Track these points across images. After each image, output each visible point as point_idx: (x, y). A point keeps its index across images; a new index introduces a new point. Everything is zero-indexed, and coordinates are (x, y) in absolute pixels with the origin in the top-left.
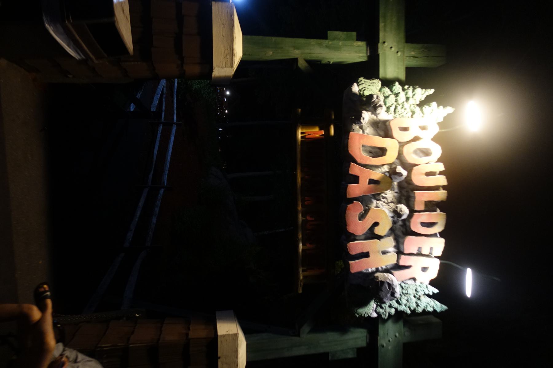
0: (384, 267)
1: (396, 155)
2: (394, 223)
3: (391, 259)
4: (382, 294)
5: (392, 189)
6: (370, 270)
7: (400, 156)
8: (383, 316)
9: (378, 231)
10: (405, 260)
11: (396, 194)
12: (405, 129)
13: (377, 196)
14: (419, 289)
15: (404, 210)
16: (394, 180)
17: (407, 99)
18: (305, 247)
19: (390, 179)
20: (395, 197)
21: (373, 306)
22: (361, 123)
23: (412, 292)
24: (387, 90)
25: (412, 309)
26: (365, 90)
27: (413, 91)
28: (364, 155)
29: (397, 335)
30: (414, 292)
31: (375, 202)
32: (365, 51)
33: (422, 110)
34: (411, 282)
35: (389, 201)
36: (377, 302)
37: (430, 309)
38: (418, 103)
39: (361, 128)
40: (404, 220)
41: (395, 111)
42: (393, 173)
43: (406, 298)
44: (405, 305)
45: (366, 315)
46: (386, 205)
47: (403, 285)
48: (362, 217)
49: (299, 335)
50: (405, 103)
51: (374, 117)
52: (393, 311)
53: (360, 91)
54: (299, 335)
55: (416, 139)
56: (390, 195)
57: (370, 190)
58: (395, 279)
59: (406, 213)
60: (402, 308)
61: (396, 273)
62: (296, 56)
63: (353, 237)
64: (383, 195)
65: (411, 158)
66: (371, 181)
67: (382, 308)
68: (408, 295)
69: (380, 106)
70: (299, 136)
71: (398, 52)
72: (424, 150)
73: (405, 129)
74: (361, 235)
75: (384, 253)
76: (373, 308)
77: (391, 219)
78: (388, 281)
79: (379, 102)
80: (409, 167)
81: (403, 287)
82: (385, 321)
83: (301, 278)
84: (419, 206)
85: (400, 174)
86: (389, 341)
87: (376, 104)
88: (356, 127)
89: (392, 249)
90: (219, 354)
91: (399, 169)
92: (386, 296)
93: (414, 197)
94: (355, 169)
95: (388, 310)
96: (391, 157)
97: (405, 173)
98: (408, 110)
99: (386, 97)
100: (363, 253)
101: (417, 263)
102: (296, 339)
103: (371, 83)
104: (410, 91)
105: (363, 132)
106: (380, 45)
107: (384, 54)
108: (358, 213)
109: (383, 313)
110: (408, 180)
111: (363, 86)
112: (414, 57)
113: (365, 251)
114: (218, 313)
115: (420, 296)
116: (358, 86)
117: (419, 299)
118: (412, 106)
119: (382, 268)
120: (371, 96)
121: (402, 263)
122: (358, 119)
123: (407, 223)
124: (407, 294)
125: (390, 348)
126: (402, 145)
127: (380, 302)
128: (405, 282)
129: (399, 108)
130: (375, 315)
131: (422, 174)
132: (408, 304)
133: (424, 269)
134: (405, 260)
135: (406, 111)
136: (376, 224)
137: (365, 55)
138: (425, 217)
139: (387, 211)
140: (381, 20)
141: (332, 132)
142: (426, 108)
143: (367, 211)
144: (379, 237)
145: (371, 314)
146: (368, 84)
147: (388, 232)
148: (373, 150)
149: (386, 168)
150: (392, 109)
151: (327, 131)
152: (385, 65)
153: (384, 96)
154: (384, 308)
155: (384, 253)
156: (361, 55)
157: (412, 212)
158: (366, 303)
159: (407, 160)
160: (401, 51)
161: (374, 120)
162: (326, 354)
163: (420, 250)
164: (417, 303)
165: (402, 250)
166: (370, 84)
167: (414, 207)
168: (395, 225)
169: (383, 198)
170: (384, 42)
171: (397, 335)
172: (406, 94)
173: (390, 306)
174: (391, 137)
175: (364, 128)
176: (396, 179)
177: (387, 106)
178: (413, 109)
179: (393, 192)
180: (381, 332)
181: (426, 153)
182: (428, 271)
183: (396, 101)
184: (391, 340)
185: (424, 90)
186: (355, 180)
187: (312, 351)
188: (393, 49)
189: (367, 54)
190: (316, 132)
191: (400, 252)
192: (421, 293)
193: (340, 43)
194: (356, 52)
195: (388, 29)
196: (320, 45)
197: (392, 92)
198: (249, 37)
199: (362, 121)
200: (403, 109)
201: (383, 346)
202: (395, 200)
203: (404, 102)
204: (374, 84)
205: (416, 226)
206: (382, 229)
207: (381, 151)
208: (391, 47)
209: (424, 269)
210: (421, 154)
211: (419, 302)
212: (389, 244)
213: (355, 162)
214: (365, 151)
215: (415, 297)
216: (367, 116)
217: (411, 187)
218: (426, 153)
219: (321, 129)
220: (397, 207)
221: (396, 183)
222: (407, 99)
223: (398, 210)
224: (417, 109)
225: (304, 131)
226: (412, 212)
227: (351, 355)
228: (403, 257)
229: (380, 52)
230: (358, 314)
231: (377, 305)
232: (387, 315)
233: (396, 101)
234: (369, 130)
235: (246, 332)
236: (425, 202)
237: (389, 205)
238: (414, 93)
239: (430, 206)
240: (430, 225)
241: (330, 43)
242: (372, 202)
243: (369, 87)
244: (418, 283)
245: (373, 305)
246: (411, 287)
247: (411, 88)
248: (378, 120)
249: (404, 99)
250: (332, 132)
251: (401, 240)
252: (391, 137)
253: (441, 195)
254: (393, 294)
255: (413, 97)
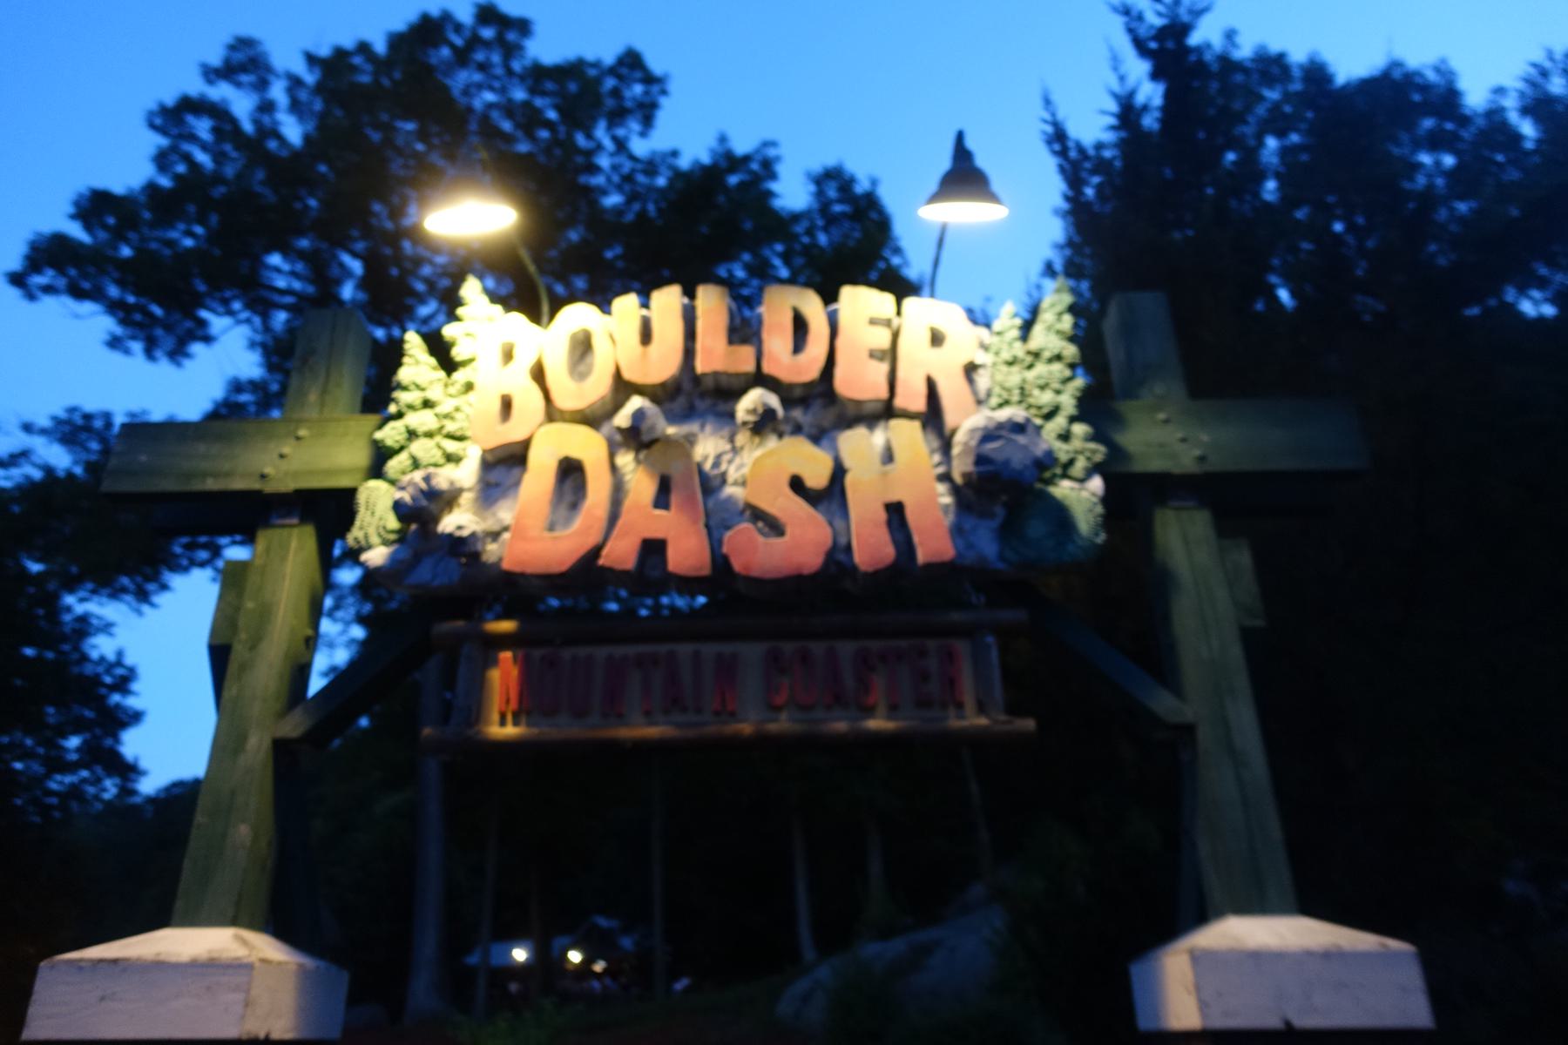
0: (937, 458)
1: (584, 431)
2: (797, 430)
3: (907, 436)
4: (1018, 460)
5: (690, 440)
6: (947, 500)
7: (592, 419)
8: (1098, 458)
9: (817, 474)
10: (912, 397)
11: (708, 428)
12: (507, 405)
13: (710, 485)
14: (1006, 355)
15: (752, 400)
16: (657, 434)
17: (427, 404)
18: (882, 709)
19: (656, 448)
20: (714, 433)
21: (1067, 492)
22: (473, 535)
23: (1014, 377)
24: (394, 465)
25: (1068, 373)
26: (384, 528)
27: (405, 388)
28: (578, 522)
29: (1161, 416)
30: (1015, 369)
31: (730, 490)
32: (285, 532)
33: (463, 364)
34: (983, 381)
35: (728, 447)
36: (1055, 476)
37: (1067, 322)
38: (442, 374)
39: (495, 536)
40: (787, 402)
41: (460, 438)
42: (636, 438)
43: (1036, 392)
44: (1058, 392)
45: (1099, 509)
46: (93, 314)
47: (994, 401)
48: (774, 527)
49: (1188, 730)
50: (438, 410)
51: (466, 499)
52: (1079, 429)
53: (385, 543)
54: (1188, 730)
55: (539, 374)
56: (708, 446)
57: (689, 501)
58: (966, 421)
59: (761, 396)
60: (1068, 402)
61: (950, 418)
62: (267, 743)
63: (838, 557)
64: (708, 466)
65: (597, 387)
66: (663, 498)
67: (1071, 462)
68: (1027, 387)
69: (427, 479)
70: (510, 731)
71: (298, 438)
72: (578, 353)
73: (507, 405)
74: (828, 531)
75: (888, 456)
76: (1072, 489)
77: (789, 441)
78: (973, 443)
79: (415, 485)
80: (623, 388)
81: (1000, 401)
82: (1116, 452)
83: (983, 721)
84: (742, 360)
85: (639, 415)
86: (1183, 440)
87: (422, 491)
88: (492, 551)
89: (878, 437)
90: (1272, 1022)
91: (623, 419)
92: (1025, 447)
93: (716, 374)
94: (621, 553)
95: (1077, 444)
96: (588, 446)
97: (636, 402)
98: (462, 401)
99: (416, 464)
100: (889, 523)
101: (917, 362)
102: (1205, 736)
103: (367, 509)
104: (403, 397)
105: (506, 529)
106: (269, 488)
107: (296, 475)
108: (761, 539)
109: (1088, 459)
110: (663, 394)
111: (372, 531)
112: (324, 392)
113: (882, 516)
114: (1144, 1023)
115: (1029, 353)
116: (369, 547)
117: (1036, 355)
118: (452, 390)
119: (939, 464)
120: (398, 507)
121: (919, 404)
122: (459, 545)
123: (798, 393)
124: (1022, 389)
125: (1205, 438)
126: (552, 414)
127: (1047, 466)
128: (982, 394)
129: (450, 427)
130: (1096, 484)
131: (644, 356)
132: (1056, 386)
133: (937, 339)
134: (912, 397)
135: (465, 408)
136: (797, 484)
137: (295, 531)
138: (777, 342)
139: (758, 453)
140: (197, 486)
141: (507, 626)
142: (457, 353)
143: (757, 514)
144: (839, 472)
145: (1094, 494)
146: (368, 519)
147: (824, 449)
148: (569, 498)
149: (626, 460)
150: (452, 446)
151: (503, 641)
152: (311, 473)
153: (411, 471)
154: (1071, 456)
155: (888, 456)
156: (294, 544)
157: (760, 379)
158: (1060, 514)
159: (602, 398)
160: (297, 429)
161: (476, 500)
162: (1249, 638)
163: (879, 354)
164: (1051, 360)
165: (879, 407)
166: (369, 513)
167: (746, 374)
168: (806, 429)
169: (716, 464)
170: (263, 476)
171: (1161, 416)
172: (411, 407)
173: (1065, 437)
174: (525, 445)
175: (496, 528)
176: (652, 428)
177: (442, 461)
178: (458, 387)
179: (701, 437)
180: (1156, 465)
181: (583, 346)
182: (942, 327)
183: (429, 435)
184: (1179, 435)
185: (406, 360)
186: (653, 549)
187: (1242, 682)
188: (286, 450)
189: (291, 526)
190: (503, 676)
191: (887, 411)
192: (1019, 349)
193: (250, 605)
194: (283, 559)
195: (227, 466)
196: (243, 668)
197: (402, 448)
198: (179, 905)
199: (465, 533)
200: (458, 415)
201: (1202, 459)
202: (726, 432)
203: (436, 415)
204: (371, 501)
205: (808, 366)
206: (814, 465)
207: (570, 471)
208: (282, 456)
209: (937, 339)
210: (588, 360)
211: (1047, 354)
212: (860, 445)
213: (596, 551)
214: (568, 521)
215: (1030, 367)
216: (457, 521)
217: (687, 386)
218: (583, 346)
219: (492, 662)
220: (745, 423)
221: (671, 430)
222: (427, 404)
223: (752, 418)
224: (460, 376)
225: (495, 717)
226: (760, 379)
227: (1243, 558)
228: (899, 402)
229: (290, 486)
230: (1097, 535)
231: (1065, 476)
232: (1092, 445)
233: (429, 435)
234: (505, 513)
235: (1202, 916)
236: (731, 342)
237: (742, 448)
238: (412, 387)
239: (744, 330)
240: (800, 326)
241: (243, 636)
242: (730, 499)
243: (378, 514)
244: (980, 358)
245: (1063, 489)
246: (999, 377)
247: (398, 394)
248: (478, 487)
249: (428, 413)
250: (507, 626)
251: (851, 411)
252: (525, 445)
253: (711, 303)
254: (1019, 428)
255: (423, 389)
